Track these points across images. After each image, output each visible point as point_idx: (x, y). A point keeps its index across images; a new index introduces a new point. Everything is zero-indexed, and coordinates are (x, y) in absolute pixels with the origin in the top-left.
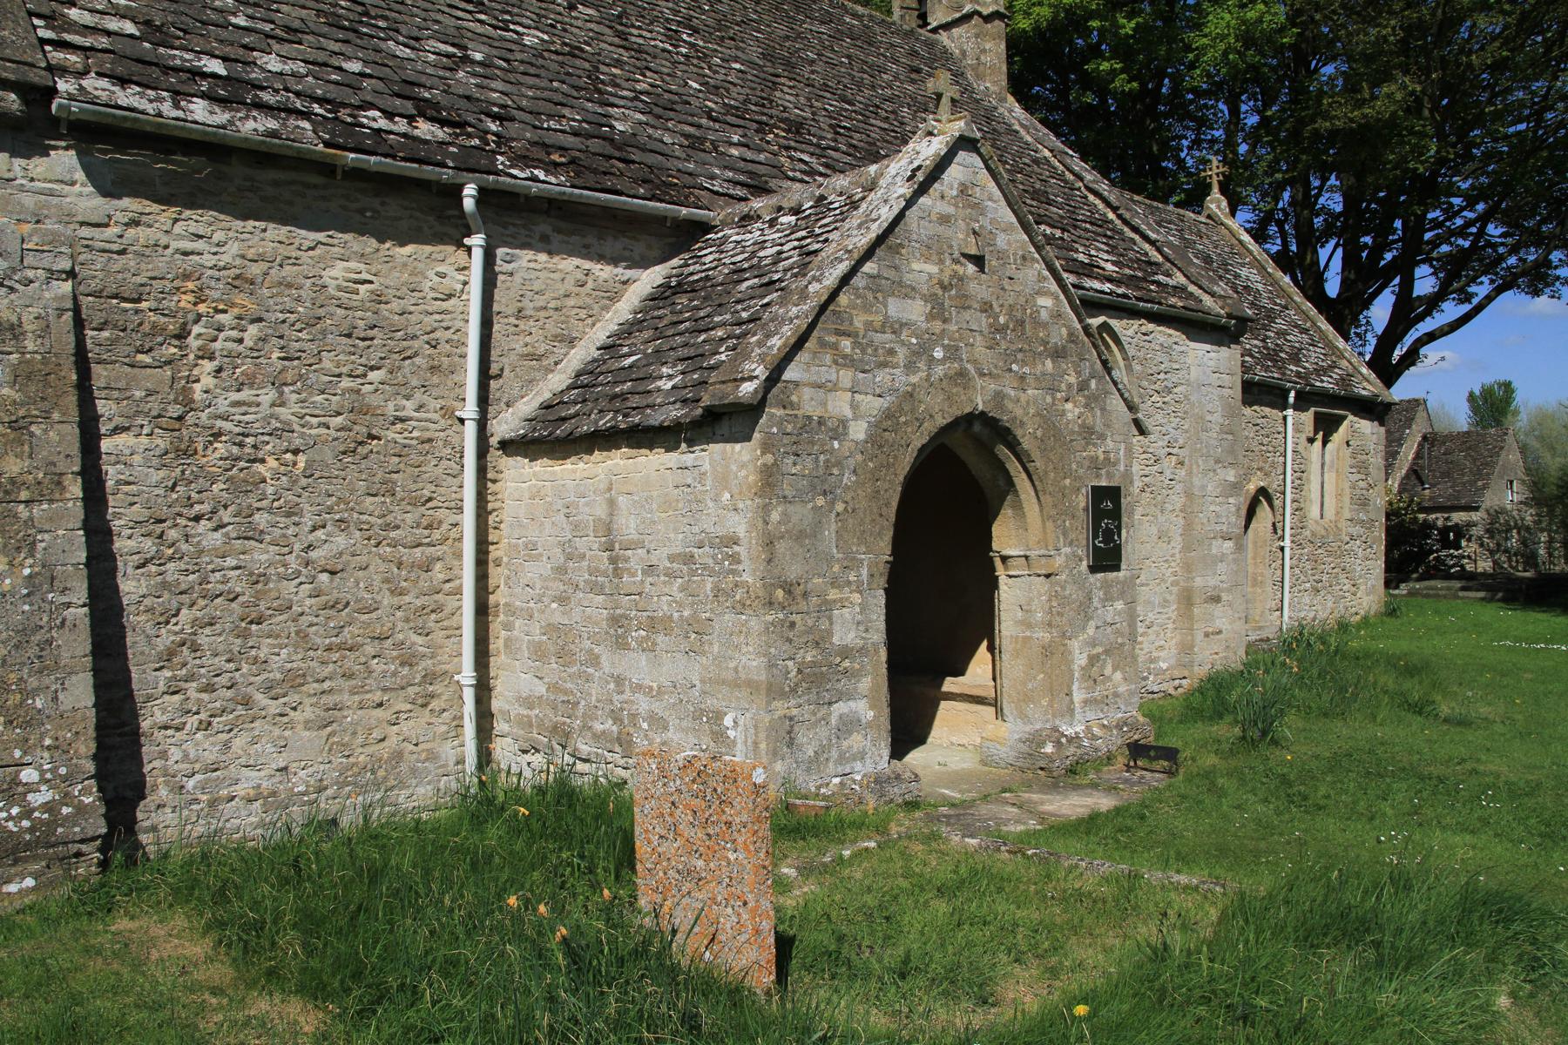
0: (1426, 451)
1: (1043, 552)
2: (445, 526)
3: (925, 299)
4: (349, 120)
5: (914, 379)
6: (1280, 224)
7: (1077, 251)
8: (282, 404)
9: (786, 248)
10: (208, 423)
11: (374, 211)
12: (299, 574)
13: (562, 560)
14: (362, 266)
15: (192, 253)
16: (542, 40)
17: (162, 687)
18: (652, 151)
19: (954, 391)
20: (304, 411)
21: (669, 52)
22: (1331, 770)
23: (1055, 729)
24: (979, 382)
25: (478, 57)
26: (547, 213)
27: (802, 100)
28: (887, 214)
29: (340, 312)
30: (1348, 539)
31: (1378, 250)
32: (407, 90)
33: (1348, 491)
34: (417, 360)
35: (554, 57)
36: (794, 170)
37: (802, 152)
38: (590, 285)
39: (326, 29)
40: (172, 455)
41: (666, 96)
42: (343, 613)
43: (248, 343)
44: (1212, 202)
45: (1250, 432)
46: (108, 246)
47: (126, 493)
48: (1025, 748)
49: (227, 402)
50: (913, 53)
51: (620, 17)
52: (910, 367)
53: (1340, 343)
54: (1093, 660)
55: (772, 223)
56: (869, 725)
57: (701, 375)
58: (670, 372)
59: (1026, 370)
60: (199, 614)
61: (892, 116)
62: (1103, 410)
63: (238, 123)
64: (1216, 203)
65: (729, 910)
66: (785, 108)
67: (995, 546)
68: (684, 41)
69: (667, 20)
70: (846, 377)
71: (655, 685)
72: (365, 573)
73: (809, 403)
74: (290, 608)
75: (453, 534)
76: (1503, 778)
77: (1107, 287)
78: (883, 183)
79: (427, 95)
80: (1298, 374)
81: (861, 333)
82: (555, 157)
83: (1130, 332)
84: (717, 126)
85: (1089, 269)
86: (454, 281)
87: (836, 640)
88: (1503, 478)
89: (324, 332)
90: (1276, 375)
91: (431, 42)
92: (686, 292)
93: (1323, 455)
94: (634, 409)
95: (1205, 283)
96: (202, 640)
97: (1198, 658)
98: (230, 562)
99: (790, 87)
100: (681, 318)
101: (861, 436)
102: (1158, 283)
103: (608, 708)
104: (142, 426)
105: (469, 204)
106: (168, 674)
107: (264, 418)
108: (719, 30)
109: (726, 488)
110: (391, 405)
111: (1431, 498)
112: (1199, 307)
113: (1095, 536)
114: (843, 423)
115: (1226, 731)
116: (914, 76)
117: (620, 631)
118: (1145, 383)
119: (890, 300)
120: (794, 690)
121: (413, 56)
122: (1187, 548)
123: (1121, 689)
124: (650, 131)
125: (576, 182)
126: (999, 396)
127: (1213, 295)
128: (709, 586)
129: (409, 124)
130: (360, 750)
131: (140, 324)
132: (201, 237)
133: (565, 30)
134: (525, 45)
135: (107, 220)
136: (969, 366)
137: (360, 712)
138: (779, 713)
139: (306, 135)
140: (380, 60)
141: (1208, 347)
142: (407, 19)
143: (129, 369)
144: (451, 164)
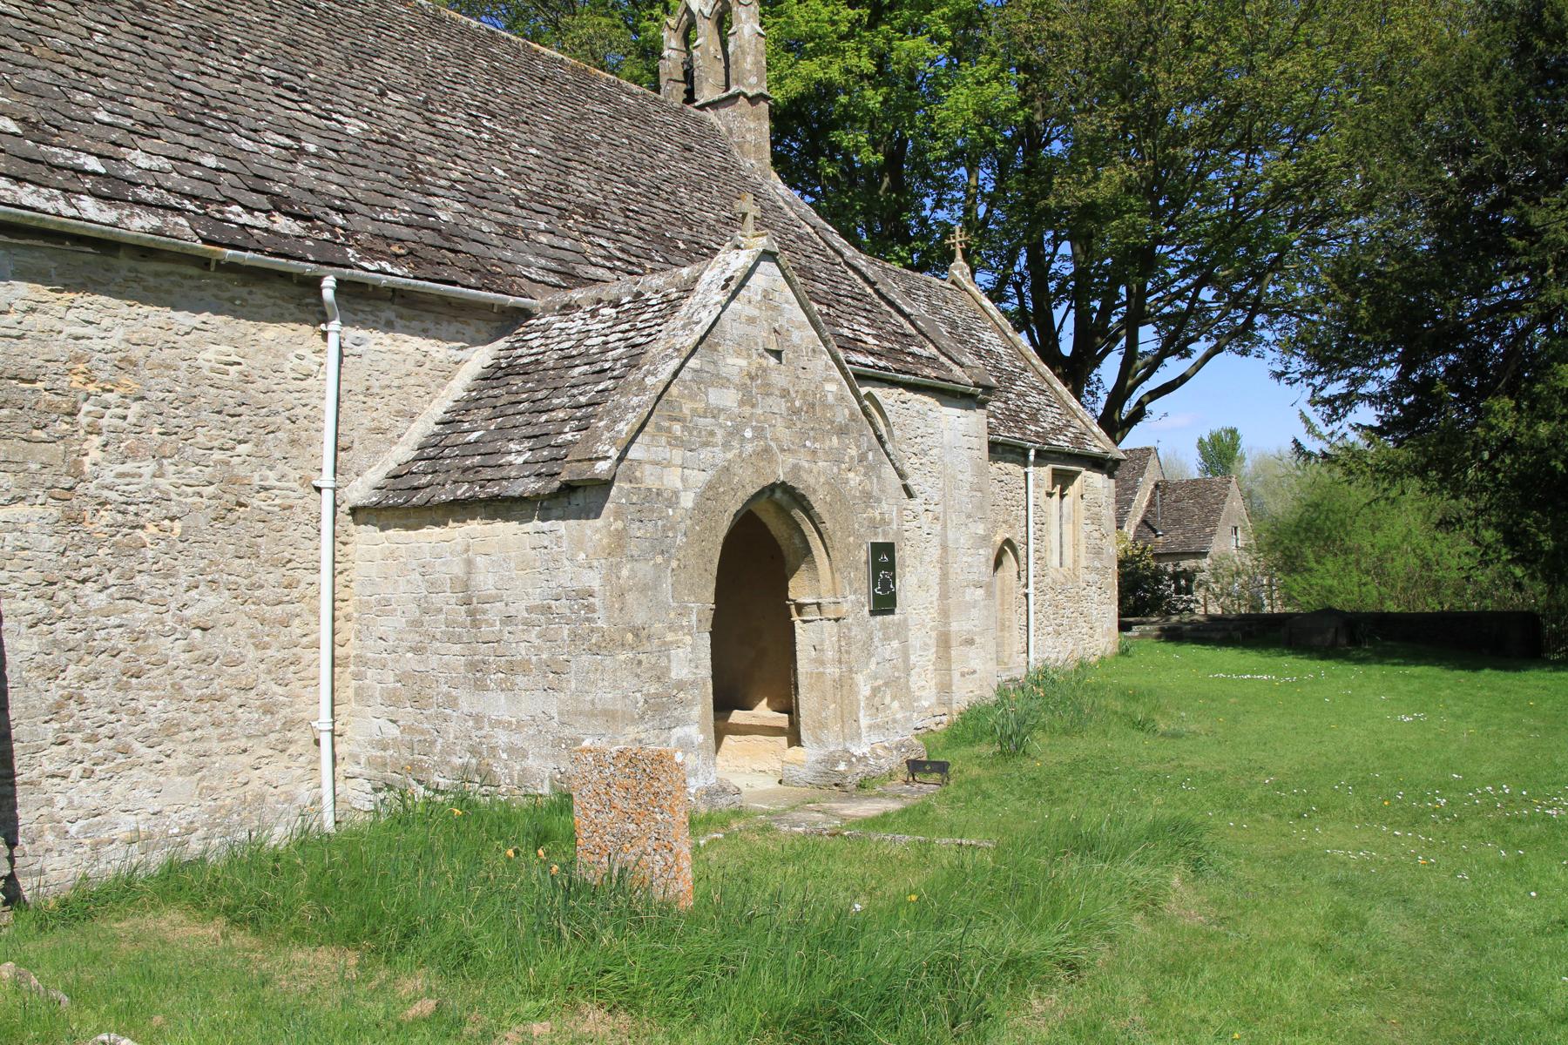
0: (1158, 498)
1: (832, 600)
2: (303, 585)
3: (737, 387)
4: (218, 216)
5: (729, 455)
6: (1018, 286)
7: (842, 326)
8: (162, 476)
9: (611, 338)
10: (97, 493)
11: (244, 300)
12: (175, 630)
13: (418, 614)
14: (232, 350)
15: (83, 338)
16: (363, 129)
17: (50, 738)
18: (474, 240)
19: (761, 464)
20: (180, 482)
21: (473, 138)
22: (1071, 772)
23: (846, 751)
24: (780, 457)
25: (312, 148)
26: (391, 300)
27: (594, 185)
28: (707, 319)
29: (212, 390)
30: (1084, 585)
31: (1105, 312)
32: (259, 184)
33: (1083, 540)
34: (279, 434)
35: (375, 146)
36: (595, 256)
37: (600, 236)
38: (428, 365)
39: (177, 123)
40: (64, 523)
41: (478, 184)
42: (213, 666)
43: (132, 419)
44: (956, 269)
45: (996, 488)
46: (9, 332)
47: (23, 559)
48: (821, 768)
49: (112, 474)
50: (685, 132)
51: (425, 102)
52: (726, 446)
53: (1074, 403)
54: (875, 690)
55: (594, 314)
56: (700, 747)
57: (550, 453)
58: (519, 448)
59: (817, 445)
60: (85, 670)
61: (672, 198)
62: (879, 477)
63: (126, 221)
64: (959, 268)
65: (658, 857)
66: (580, 192)
67: (791, 596)
68: (485, 127)
69: (467, 104)
70: (677, 455)
71: (514, 720)
72: (233, 629)
73: (650, 478)
74: (166, 662)
75: (311, 591)
76: (1199, 769)
77: (870, 360)
78: (699, 287)
79: (277, 189)
80: (1037, 434)
81: (689, 419)
82: (395, 249)
83: (891, 401)
84: (524, 213)
85: (852, 344)
86: (311, 363)
87: (673, 675)
88: (1227, 524)
89: (198, 409)
90: (1017, 435)
91: (269, 134)
92: (519, 374)
93: (1061, 507)
94: (489, 481)
95: (954, 354)
96: (87, 693)
97: (956, 697)
98: (114, 620)
99: (581, 171)
100: (519, 399)
101: (690, 505)
102: (913, 355)
103: (466, 744)
104: (37, 496)
105: (328, 294)
106: (57, 726)
107: (145, 488)
108: (513, 114)
109: (581, 549)
110: (256, 476)
111: (1164, 545)
112: (950, 377)
113: (875, 586)
114: (676, 493)
115: (986, 749)
116: (687, 154)
117: (478, 675)
118: (904, 447)
119: (710, 390)
120: (642, 718)
121: (256, 149)
122: (944, 596)
123: (899, 716)
124: (469, 220)
125: (419, 273)
126: (796, 468)
127: (961, 365)
128: (566, 632)
129: (268, 218)
130: (227, 793)
131: (37, 403)
132: (91, 323)
133: (380, 118)
134: (348, 135)
135: (6, 308)
136: (772, 444)
137: (226, 758)
138: (631, 737)
139: (183, 231)
140: (230, 154)
141: (958, 412)
142: (243, 110)
143: (26, 444)
144: (311, 258)
